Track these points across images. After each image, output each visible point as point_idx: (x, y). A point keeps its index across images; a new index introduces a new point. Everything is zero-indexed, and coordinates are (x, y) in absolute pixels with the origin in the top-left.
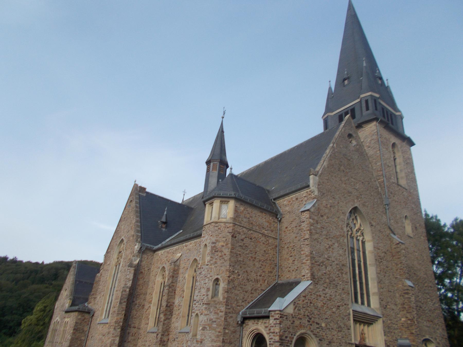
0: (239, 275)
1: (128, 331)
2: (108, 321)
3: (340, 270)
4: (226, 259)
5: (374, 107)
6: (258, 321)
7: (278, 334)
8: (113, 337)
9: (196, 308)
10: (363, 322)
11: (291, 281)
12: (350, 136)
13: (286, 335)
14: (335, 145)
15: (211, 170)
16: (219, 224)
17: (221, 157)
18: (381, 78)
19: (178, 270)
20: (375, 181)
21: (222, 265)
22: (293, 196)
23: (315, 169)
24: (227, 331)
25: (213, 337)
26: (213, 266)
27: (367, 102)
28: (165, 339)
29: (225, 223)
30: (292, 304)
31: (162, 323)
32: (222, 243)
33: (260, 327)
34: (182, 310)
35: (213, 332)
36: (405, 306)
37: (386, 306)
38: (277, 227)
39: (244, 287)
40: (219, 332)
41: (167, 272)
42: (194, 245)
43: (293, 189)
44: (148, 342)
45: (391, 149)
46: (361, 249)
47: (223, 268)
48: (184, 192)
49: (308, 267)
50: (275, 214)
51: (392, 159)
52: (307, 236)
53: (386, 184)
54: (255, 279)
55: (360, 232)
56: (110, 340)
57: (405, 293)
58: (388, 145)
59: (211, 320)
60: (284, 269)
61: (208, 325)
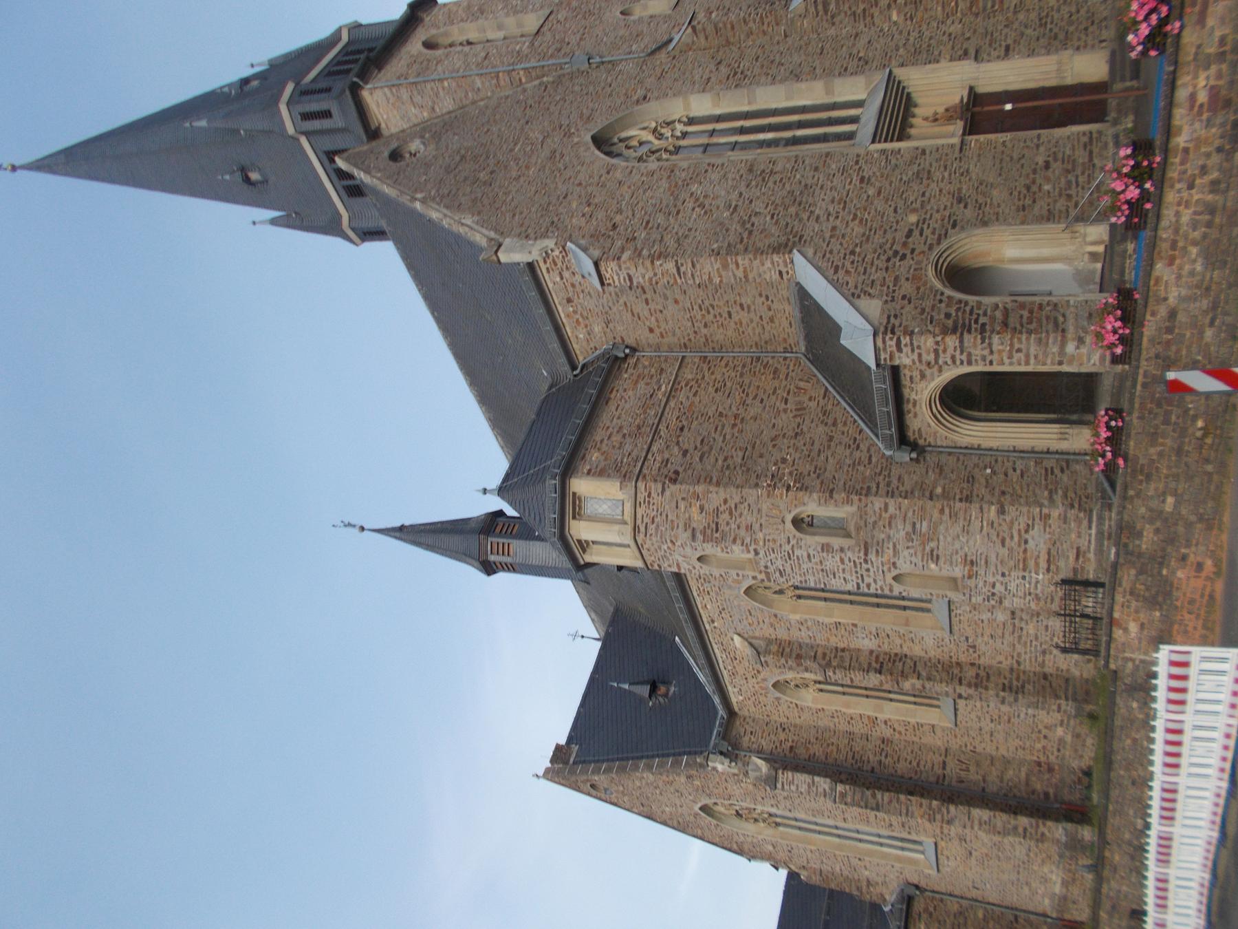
0: (784, 461)
1: (954, 783)
2: (929, 842)
3: (764, 177)
4: (737, 499)
5: (316, 96)
6: (908, 400)
7: (939, 339)
8: (972, 828)
9: (879, 583)
10: (905, 119)
11: (797, 314)
12: (395, 156)
13: (942, 316)
14: (419, 196)
16: (639, 522)
17: (472, 531)
18: (245, 81)
19: (780, 643)
20: (525, 90)
21: (754, 507)
22: (562, 311)
23: (481, 249)
24: (939, 490)
25: (957, 529)
26: (760, 535)
27: (306, 116)
28: (970, 673)
29: (635, 505)
30: (857, 302)
31: (928, 685)
32: (695, 510)
33: (923, 392)
34: (888, 628)
35: (942, 528)
36: (859, 11)
37: (860, 59)
38: (651, 358)
39: (816, 447)
40: (942, 511)
41: (790, 675)
42: (707, 597)
43: (542, 311)
44: (983, 724)
45: (439, 53)
46: (710, 127)
47: (764, 507)
49: (756, 263)
50: (613, 363)
51: (467, 49)
52: (670, 266)
53: (533, 63)
54: (795, 417)
55: (663, 131)
56: (981, 834)
57: (826, 12)
58: (429, 61)
59: (909, 538)
60: (766, 336)
61: (923, 544)
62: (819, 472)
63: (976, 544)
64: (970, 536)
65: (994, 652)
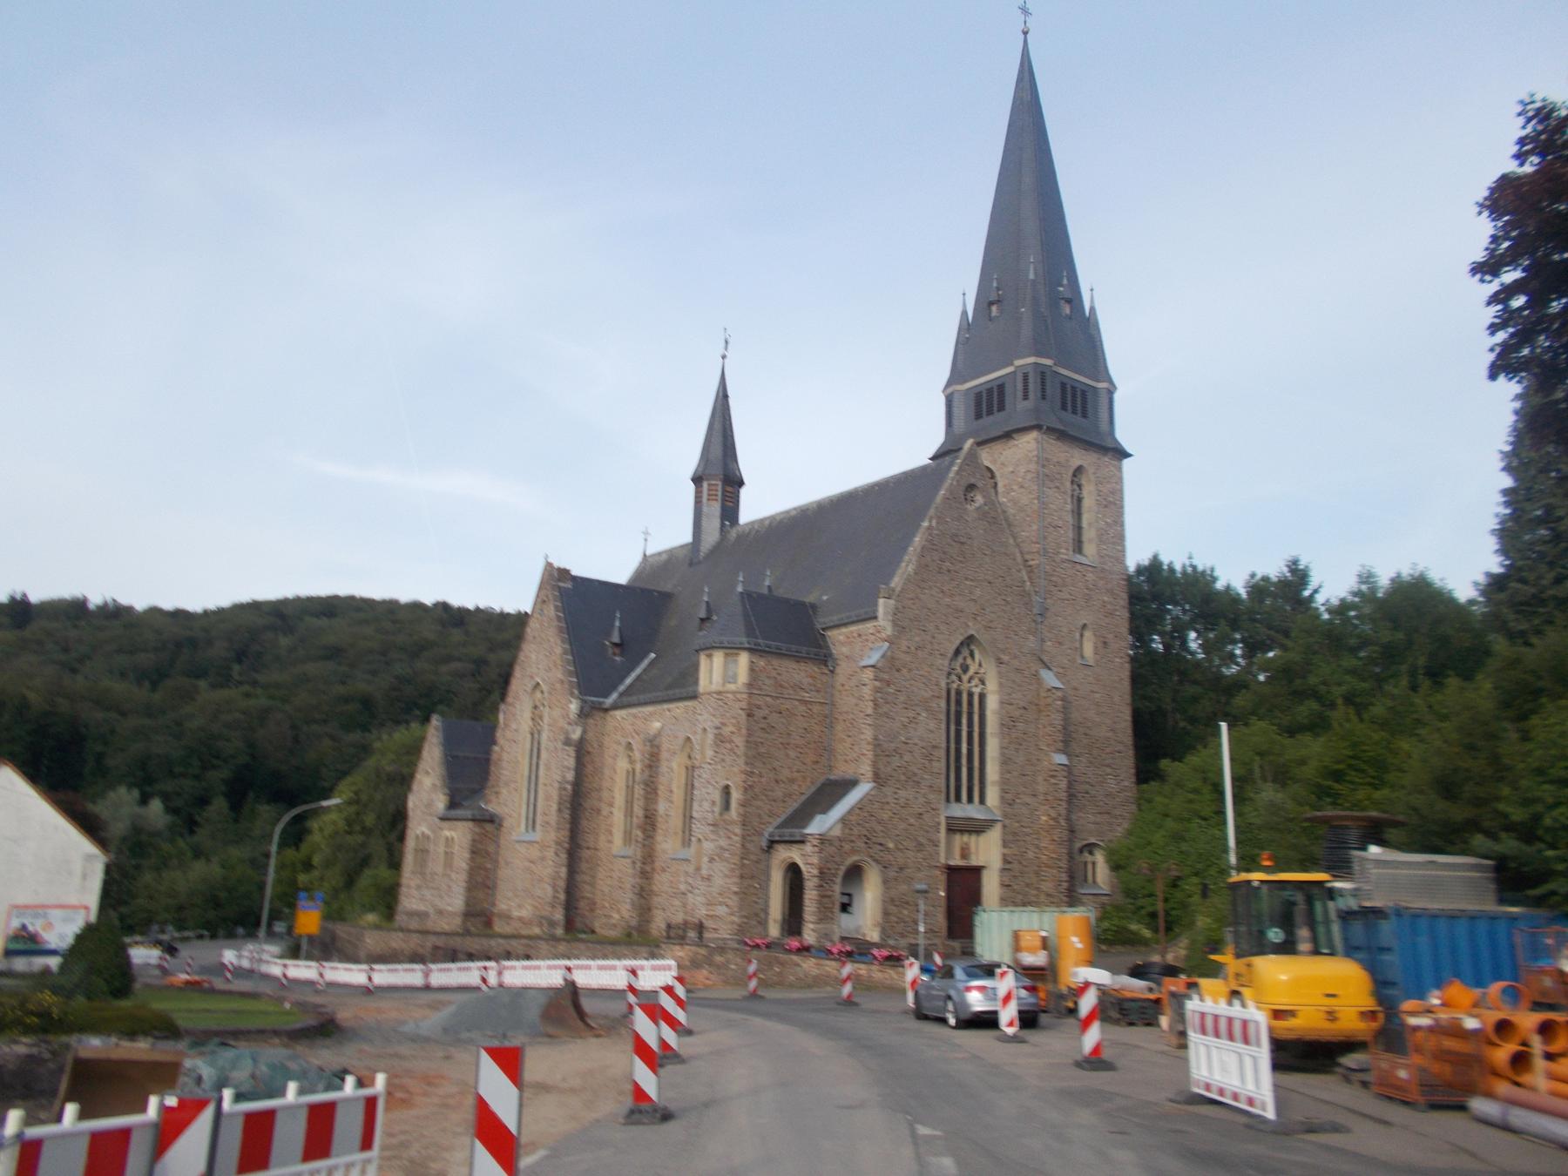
2: (537, 836)
14: (934, 523)
15: (705, 499)
17: (725, 465)
28: (648, 868)
29: (734, 693)
32: (731, 728)
33: (794, 854)
48: (646, 533)
50: (822, 656)
52: (870, 711)
59: (722, 848)
62: (756, 797)
63: (719, 881)
64: (722, 878)
65: (661, 882)
